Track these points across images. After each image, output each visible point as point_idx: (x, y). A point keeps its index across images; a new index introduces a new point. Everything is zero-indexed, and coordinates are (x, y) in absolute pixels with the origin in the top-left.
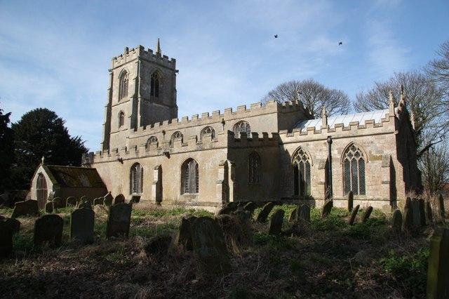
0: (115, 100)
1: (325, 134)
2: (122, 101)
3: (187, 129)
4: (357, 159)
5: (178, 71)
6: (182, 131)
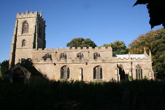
0: (19, 33)
1: (130, 60)
2: (24, 34)
3: (69, 53)
4: (138, 69)
5: (46, 26)
6: (67, 54)
